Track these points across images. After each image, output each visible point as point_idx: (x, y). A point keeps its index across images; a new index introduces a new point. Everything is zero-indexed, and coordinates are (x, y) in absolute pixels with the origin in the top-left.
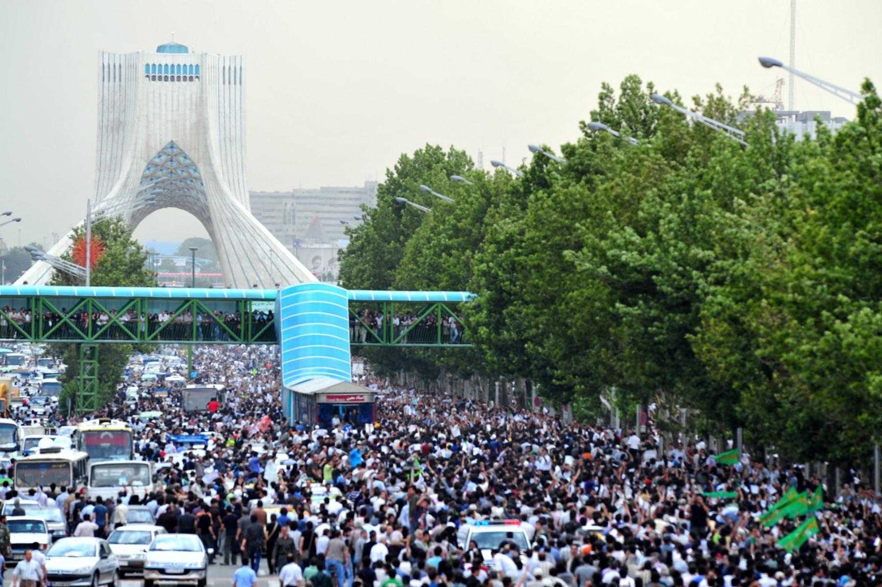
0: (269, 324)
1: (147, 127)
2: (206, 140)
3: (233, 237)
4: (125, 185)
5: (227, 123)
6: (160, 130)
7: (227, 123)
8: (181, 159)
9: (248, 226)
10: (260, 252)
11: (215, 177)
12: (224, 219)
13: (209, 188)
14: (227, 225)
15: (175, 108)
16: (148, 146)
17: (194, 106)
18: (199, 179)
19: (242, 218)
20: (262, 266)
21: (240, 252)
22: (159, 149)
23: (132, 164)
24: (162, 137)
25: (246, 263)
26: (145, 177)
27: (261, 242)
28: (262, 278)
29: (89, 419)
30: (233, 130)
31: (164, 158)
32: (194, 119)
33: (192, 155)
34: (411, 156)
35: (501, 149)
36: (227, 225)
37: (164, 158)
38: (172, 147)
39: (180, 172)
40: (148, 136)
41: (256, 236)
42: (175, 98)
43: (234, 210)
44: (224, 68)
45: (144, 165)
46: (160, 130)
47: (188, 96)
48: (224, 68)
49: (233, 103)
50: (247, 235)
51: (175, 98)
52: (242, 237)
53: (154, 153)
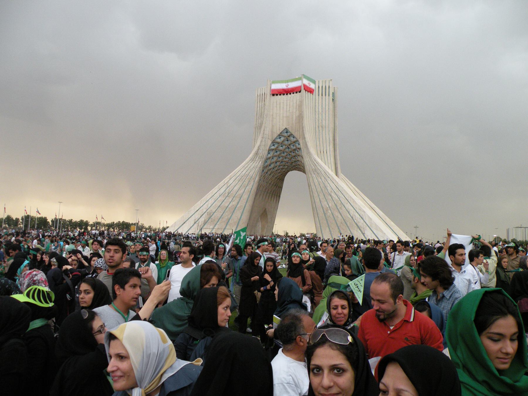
0: (506, 311)
1: (272, 121)
2: (302, 124)
3: (316, 180)
4: (257, 153)
5: (320, 117)
6: (280, 122)
7: (320, 117)
8: (292, 138)
9: (323, 172)
10: (329, 188)
11: (306, 144)
12: (311, 170)
13: (304, 153)
14: (312, 173)
15: (288, 109)
16: (272, 132)
17: (298, 107)
18: (300, 149)
19: (320, 168)
20: (330, 198)
21: (319, 190)
22: (279, 133)
23: (261, 141)
24: (280, 126)
25: (322, 196)
26: (270, 150)
27: (330, 182)
28: (330, 205)
29: (293, 93)
30: (324, 122)
31: (282, 139)
32: (297, 114)
33: (295, 134)
34: (121, 222)
35: (74, 220)
36: (312, 173)
37: (282, 139)
38: (287, 132)
39: (292, 147)
40: (273, 126)
41: (327, 178)
42: (288, 104)
43: (315, 163)
44: (319, 87)
45: (269, 143)
46: (280, 122)
47: (295, 102)
48: (319, 87)
49: (324, 106)
50: (323, 178)
51: (288, 104)
52: (320, 180)
53: (275, 136)
